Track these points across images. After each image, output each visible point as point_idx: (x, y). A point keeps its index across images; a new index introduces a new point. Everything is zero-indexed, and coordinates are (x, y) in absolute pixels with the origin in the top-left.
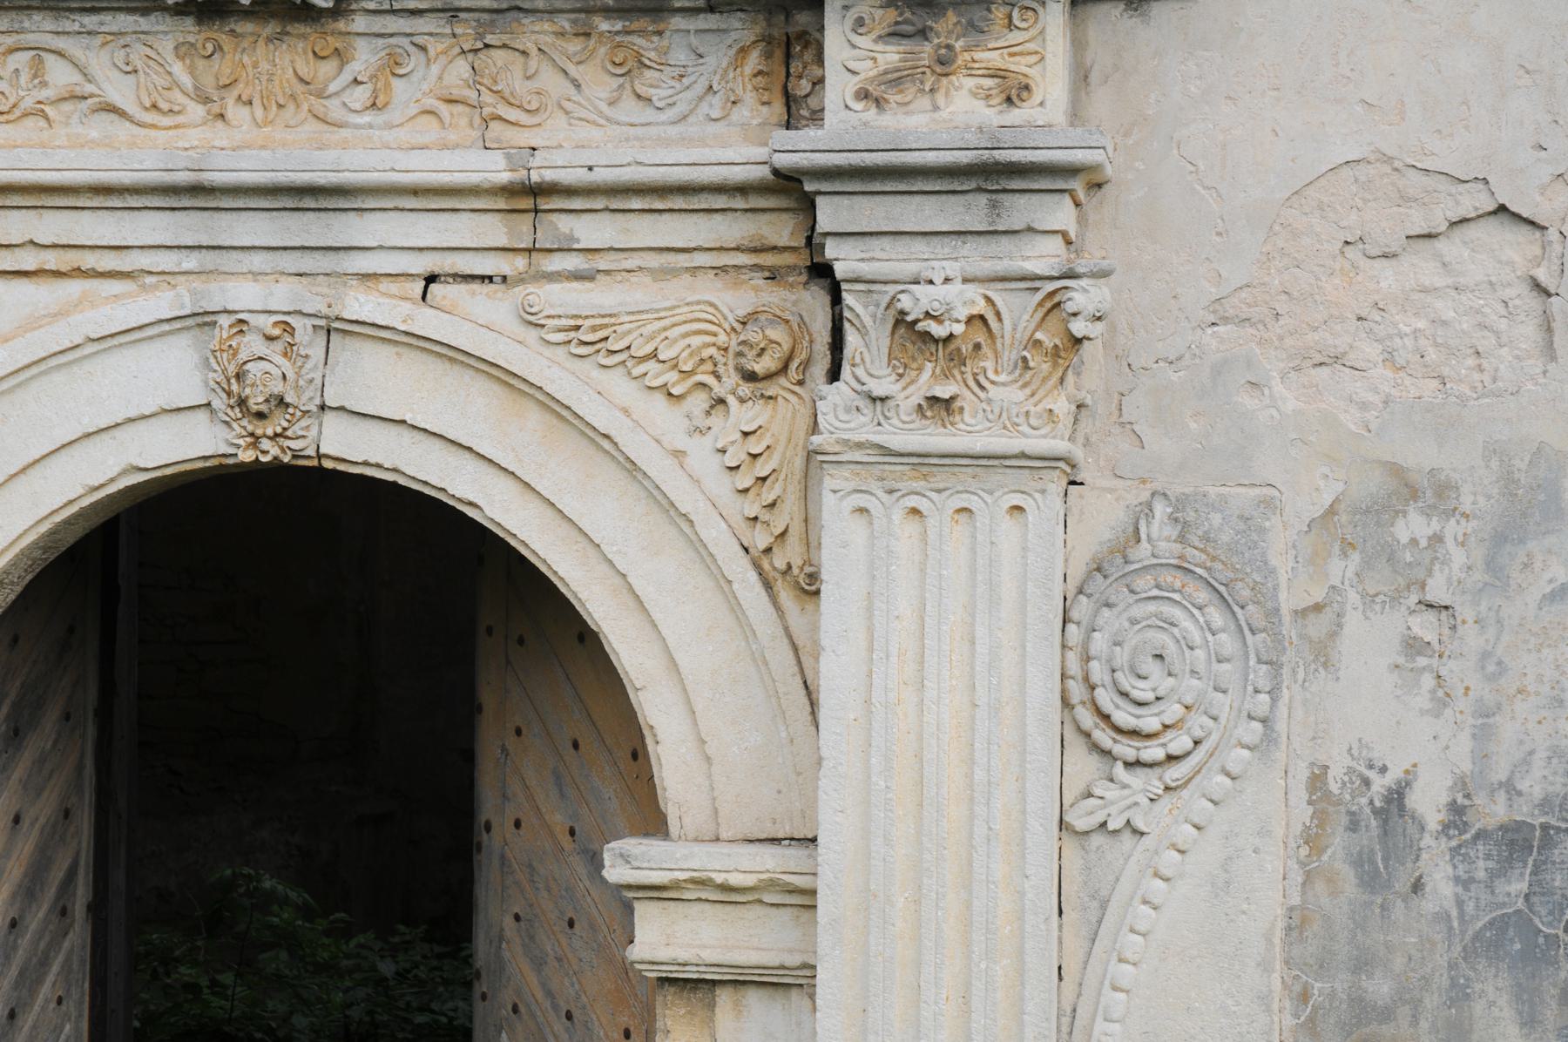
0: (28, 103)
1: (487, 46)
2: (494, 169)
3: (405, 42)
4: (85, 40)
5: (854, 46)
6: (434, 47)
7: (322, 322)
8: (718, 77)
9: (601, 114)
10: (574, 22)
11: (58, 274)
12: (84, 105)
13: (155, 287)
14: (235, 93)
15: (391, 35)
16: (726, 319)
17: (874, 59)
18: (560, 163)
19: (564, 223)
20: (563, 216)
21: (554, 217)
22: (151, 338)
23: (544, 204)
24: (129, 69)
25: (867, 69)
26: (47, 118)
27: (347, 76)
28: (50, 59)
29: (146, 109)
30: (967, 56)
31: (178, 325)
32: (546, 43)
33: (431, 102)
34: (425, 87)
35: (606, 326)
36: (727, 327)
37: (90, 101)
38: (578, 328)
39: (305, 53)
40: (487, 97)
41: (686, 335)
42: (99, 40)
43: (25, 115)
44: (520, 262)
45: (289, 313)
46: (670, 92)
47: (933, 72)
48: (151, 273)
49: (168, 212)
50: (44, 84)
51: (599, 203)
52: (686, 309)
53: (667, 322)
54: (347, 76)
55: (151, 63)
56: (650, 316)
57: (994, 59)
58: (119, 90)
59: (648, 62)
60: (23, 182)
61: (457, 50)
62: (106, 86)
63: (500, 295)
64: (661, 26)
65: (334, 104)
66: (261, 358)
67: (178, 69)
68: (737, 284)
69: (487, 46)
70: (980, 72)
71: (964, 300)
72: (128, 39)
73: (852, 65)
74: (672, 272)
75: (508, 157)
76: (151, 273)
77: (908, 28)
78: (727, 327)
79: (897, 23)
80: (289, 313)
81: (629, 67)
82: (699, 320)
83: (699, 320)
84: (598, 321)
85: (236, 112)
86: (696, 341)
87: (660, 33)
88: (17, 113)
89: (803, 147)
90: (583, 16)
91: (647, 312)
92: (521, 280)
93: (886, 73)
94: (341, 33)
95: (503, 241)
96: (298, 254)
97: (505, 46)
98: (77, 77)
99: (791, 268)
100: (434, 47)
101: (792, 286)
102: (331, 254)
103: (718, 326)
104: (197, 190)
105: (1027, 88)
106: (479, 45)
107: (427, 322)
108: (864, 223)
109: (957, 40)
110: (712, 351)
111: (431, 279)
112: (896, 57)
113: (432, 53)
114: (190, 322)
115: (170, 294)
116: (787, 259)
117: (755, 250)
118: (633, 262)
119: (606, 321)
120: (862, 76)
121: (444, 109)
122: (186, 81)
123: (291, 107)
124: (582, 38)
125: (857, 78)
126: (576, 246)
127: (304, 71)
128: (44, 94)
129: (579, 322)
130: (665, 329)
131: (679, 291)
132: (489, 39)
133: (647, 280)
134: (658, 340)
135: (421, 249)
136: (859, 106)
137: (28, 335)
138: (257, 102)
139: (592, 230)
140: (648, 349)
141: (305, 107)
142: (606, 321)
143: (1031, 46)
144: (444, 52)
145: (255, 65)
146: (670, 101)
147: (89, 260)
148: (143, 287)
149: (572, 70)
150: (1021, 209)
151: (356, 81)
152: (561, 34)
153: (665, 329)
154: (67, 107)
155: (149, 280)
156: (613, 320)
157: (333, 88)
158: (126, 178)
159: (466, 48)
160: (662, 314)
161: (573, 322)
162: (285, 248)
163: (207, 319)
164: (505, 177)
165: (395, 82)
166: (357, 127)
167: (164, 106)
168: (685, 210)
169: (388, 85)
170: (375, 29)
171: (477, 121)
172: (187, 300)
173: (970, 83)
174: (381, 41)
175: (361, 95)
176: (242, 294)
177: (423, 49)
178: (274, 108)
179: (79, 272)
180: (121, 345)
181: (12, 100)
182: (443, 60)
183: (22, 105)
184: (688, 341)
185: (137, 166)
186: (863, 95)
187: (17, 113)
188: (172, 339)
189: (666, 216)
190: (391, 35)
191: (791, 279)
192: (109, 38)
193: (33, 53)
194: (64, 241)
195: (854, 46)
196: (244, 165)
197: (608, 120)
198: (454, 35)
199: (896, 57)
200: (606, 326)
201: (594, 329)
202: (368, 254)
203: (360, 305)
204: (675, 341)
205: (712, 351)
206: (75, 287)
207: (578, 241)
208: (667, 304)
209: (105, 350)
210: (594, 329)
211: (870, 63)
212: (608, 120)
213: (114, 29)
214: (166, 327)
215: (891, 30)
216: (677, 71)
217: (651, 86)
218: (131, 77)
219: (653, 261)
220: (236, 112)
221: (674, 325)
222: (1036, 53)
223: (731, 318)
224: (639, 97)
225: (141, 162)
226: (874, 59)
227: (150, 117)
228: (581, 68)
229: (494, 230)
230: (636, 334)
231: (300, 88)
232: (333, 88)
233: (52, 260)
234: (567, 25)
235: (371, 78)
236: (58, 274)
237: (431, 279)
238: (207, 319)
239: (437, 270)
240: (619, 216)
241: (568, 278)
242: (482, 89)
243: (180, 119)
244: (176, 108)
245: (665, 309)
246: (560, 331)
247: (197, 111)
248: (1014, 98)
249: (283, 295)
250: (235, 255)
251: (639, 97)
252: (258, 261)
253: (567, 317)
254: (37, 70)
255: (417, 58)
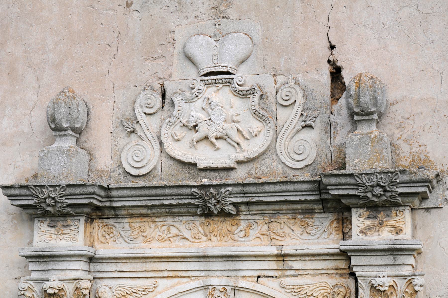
0: (166, 238)
1: (271, 222)
2: (274, 251)
3: (252, 221)
4: (179, 223)
5: (359, 221)
6: (259, 222)
7: (233, 288)
8: (326, 228)
9: (298, 237)
10: (292, 216)
11: (172, 277)
12: (179, 238)
13: (194, 280)
14: (213, 234)
15: (249, 220)
16: (329, 286)
17: (364, 224)
18: (289, 249)
19: (290, 263)
20: (290, 262)
21: (288, 262)
22: (193, 292)
23: (285, 259)
24: (189, 229)
25: (362, 226)
26: (170, 241)
27: (239, 230)
28: (171, 227)
29: (193, 238)
30: (386, 223)
31: (200, 289)
32: (285, 221)
33: (259, 235)
34: (257, 232)
35: (301, 288)
36: (330, 288)
37: (180, 237)
38: (294, 288)
39: (229, 224)
40: (272, 234)
41: (320, 290)
42: (183, 222)
43: (166, 240)
44: (280, 273)
45: (225, 286)
46: (315, 232)
47: (378, 226)
48: (193, 276)
49: (198, 262)
50: (170, 233)
51: (299, 258)
52: (320, 284)
53: (315, 287)
54: (239, 230)
55: (194, 227)
56: (311, 285)
57: (393, 223)
58: (187, 234)
59: (309, 225)
60: (165, 256)
61: (265, 223)
62: (184, 233)
63: (275, 280)
64: (313, 216)
65: (236, 236)
66: (219, 296)
67: (200, 229)
68: (332, 278)
69: (271, 222)
70: (390, 226)
71: (388, 281)
72: (189, 222)
73: (358, 225)
74: (317, 275)
75: (277, 248)
76: (193, 276)
77: (372, 216)
78: (330, 288)
79: (369, 215)
80: (225, 286)
81: (305, 226)
82: (323, 286)
83: (323, 286)
84: (299, 287)
85: (213, 238)
86: (323, 291)
87: (312, 218)
88: (164, 240)
89: (347, 245)
90: (294, 214)
91: (310, 284)
92: (280, 277)
93: (367, 227)
94: (238, 220)
95: (276, 268)
96: (228, 271)
97: (276, 222)
98: (177, 231)
99: (345, 274)
100: (259, 222)
101: (345, 278)
102: (235, 271)
103: (328, 288)
104: (204, 257)
105: (401, 230)
106: (270, 221)
107: (258, 287)
108: (363, 263)
109: (384, 219)
110: (326, 294)
111: (259, 277)
112: (369, 223)
113: (259, 224)
114: (202, 288)
115: (198, 281)
116: (344, 271)
117: (336, 269)
118: (307, 272)
119: (301, 287)
120: (361, 228)
121: (261, 237)
122: (202, 231)
123: (226, 237)
124: (294, 220)
125: (360, 228)
126: (293, 269)
127: (229, 229)
128: (170, 235)
129: (294, 287)
130: (315, 289)
131: (318, 279)
132: (272, 220)
133: (310, 277)
134: (313, 291)
135: (256, 270)
136: (360, 235)
137: (166, 292)
138: (218, 236)
139: (297, 265)
140: (311, 293)
141: (229, 237)
142: (301, 287)
143: (402, 220)
144: (262, 223)
145: (218, 227)
146: (315, 234)
147: (180, 274)
148: (192, 280)
149: (292, 227)
150: (401, 259)
151: (241, 231)
152: (289, 219)
153: (315, 289)
154: (175, 238)
155: (193, 278)
156: (302, 286)
157: (236, 232)
158: (188, 254)
159: (267, 222)
160: (314, 285)
161: (293, 287)
162: (225, 270)
163: (207, 287)
164: (276, 252)
165: (250, 231)
166: (241, 241)
167: (197, 237)
168: (319, 260)
169: (248, 231)
170: (246, 218)
171: (269, 239)
172: (202, 283)
173: (387, 229)
174: (247, 221)
175: (242, 234)
176: (215, 281)
177: (257, 223)
178: (222, 237)
179: (177, 277)
180: (186, 294)
181: (163, 237)
182: (261, 225)
183: (165, 238)
184: (320, 291)
185: (191, 252)
186: (362, 232)
187: (164, 240)
188: (198, 292)
189: (315, 261)
190: (249, 220)
191: (345, 276)
192: (185, 222)
193: (168, 226)
194: (174, 269)
195: (359, 221)
196: (215, 251)
197: (300, 238)
198: (264, 219)
199: (369, 223)
200: (301, 288)
201: (298, 289)
202: (244, 271)
203: (242, 283)
204: (317, 291)
205: (326, 294)
206: (176, 280)
207: (294, 267)
208: (315, 282)
209: (183, 295)
210: (298, 289)
211: (363, 224)
212: (300, 238)
213: (186, 220)
214: (197, 289)
215: (368, 216)
216: (317, 227)
217: (310, 230)
218: (190, 231)
219: (312, 272)
220: (213, 238)
221: (317, 288)
222: (403, 222)
223: (331, 286)
224: (307, 233)
225: (192, 251)
226: (364, 224)
227: (194, 240)
228: (294, 226)
229: (274, 265)
230: (308, 290)
231: (228, 232)
232: (236, 232)
233: (171, 274)
234: (290, 217)
235: (245, 230)
236: (172, 277)
237: (259, 277)
238: (207, 287)
239: (260, 275)
240: (303, 261)
241: (291, 276)
242: (271, 232)
243: (201, 240)
244: (200, 238)
245: (315, 284)
246: (290, 289)
247: (204, 238)
248: (398, 233)
249: (224, 281)
250: (213, 272)
251: (307, 233)
252: (218, 273)
253: (291, 286)
254: (169, 230)
255: (255, 225)
